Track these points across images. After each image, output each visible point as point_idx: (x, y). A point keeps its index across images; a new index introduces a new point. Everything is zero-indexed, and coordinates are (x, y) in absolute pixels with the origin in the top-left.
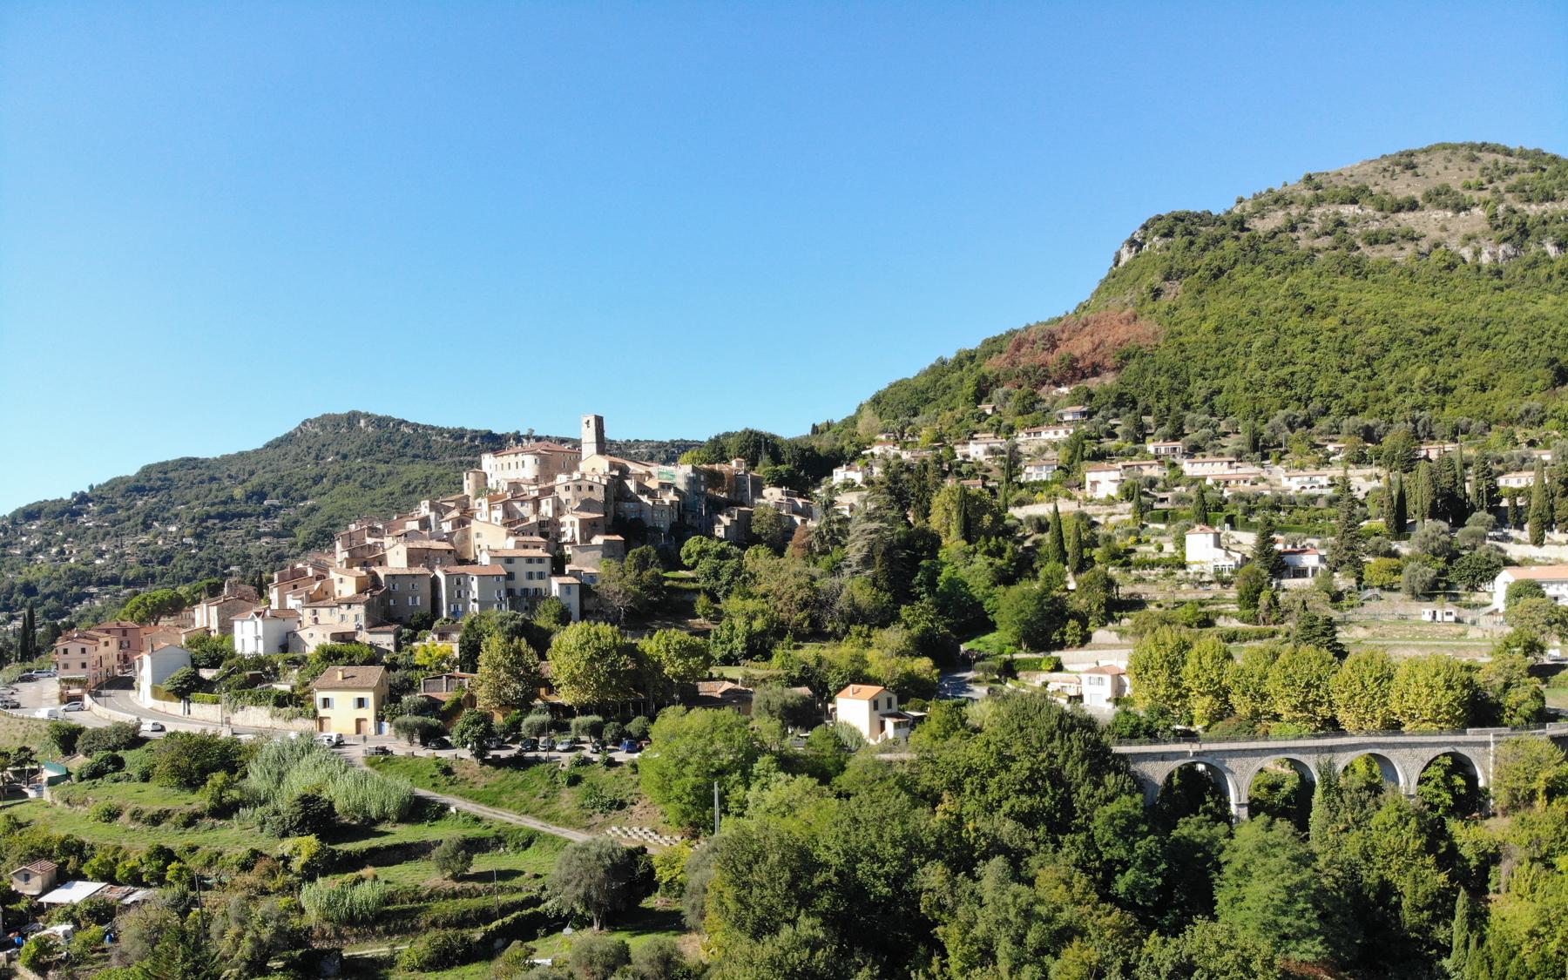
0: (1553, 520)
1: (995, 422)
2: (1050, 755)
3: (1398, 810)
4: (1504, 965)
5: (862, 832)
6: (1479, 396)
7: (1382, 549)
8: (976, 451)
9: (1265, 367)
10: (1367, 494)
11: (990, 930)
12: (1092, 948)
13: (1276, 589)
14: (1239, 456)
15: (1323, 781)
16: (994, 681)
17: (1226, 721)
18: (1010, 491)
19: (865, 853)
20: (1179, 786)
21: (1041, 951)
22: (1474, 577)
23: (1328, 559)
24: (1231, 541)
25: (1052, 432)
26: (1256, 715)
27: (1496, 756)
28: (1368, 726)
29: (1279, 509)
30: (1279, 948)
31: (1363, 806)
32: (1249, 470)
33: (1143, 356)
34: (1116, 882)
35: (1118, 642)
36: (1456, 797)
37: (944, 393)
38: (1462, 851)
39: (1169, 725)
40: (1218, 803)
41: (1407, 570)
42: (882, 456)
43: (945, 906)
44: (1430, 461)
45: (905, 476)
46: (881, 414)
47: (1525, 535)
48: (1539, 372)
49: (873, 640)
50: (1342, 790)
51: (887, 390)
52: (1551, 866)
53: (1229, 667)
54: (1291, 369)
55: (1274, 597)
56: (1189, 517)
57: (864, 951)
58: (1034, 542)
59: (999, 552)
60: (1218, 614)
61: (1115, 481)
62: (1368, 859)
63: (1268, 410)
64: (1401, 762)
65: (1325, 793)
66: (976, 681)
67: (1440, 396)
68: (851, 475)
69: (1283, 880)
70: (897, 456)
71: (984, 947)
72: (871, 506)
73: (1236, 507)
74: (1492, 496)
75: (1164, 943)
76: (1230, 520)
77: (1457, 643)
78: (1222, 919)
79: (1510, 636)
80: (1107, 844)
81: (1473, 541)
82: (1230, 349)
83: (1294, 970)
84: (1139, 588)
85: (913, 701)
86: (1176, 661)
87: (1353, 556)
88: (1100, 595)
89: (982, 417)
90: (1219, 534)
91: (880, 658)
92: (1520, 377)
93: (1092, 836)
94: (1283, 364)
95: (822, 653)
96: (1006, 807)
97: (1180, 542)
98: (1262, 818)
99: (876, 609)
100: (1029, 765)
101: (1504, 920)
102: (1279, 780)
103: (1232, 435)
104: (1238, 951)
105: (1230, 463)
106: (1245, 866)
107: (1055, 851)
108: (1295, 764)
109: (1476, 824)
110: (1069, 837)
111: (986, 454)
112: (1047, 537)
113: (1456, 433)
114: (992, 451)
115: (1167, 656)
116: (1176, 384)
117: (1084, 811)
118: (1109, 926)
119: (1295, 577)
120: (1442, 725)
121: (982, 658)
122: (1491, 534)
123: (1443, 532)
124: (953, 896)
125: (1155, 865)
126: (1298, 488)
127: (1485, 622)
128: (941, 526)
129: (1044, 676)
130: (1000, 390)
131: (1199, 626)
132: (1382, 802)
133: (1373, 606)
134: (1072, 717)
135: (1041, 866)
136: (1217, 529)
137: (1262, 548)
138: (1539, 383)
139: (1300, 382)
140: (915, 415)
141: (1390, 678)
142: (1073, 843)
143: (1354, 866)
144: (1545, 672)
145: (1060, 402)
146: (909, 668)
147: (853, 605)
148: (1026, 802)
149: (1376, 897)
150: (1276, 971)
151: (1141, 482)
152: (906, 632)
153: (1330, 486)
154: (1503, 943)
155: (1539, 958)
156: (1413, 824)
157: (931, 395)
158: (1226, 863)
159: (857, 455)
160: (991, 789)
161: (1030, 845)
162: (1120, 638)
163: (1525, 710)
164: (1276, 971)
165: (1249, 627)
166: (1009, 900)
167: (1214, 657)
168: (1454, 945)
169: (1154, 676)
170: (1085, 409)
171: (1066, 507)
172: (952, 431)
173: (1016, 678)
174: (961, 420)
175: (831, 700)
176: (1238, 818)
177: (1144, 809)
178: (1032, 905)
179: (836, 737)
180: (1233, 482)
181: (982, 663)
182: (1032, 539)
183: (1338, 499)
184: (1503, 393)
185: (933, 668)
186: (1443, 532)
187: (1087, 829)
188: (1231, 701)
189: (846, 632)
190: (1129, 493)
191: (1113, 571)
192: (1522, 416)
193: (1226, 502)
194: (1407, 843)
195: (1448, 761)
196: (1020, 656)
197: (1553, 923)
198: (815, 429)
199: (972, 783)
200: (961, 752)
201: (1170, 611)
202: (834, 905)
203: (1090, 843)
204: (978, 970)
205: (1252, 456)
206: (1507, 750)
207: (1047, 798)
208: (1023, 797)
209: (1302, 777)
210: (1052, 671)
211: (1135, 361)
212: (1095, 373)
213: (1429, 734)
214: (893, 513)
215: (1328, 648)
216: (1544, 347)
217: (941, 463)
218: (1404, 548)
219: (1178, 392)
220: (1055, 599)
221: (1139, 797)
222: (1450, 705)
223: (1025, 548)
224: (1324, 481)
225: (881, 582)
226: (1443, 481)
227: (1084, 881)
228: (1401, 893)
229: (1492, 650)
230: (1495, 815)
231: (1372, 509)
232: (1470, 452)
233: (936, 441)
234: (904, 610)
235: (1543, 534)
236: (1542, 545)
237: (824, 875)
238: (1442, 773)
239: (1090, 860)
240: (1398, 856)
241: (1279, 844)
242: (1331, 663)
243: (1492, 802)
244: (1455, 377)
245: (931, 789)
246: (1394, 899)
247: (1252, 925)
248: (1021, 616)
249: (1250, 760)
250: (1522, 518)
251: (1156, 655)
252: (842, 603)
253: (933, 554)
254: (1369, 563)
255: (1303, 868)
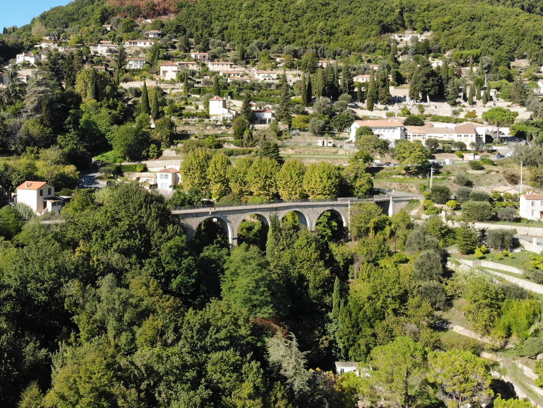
0: (378, 99)
1: (112, 35)
2: (140, 217)
3: (307, 238)
4: (357, 314)
5: (30, 266)
6: (347, 38)
7: (300, 111)
8: (102, 50)
9: (249, 17)
10: (294, 83)
11: (104, 315)
12: (159, 319)
13: (252, 130)
14: (235, 62)
15: (272, 225)
16: (111, 178)
17: (227, 196)
18: (120, 74)
19: (32, 278)
20: (204, 230)
21: (131, 324)
22: (341, 125)
23: (276, 115)
24: (231, 104)
25: (142, 43)
26: (241, 193)
27: (351, 211)
28: (294, 197)
29: (254, 90)
30: (252, 312)
31: (291, 236)
32: (240, 69)
33: (189, 6)
34: (171, 283)
35: (176, 156)
36: (333, 232)
37: (83, 16)
38: (336, 258)
39: (200, 199)
40: (223, 238)
41: (311, 121)
42: (47, 49)
43: (78, 304)
44: (323, 68)
45: (60, 61)
46: (46, 25)
47: (365, 105)
48: (374, 27)
49: (40, 155)
50: (281, 229)
51: (50, 12)
52: (377, 265)
53: (229, 169)
54: (261, 19)
55: (251, 134)
56: (211, 92)
57: (31, 333)
58: (133, 102)
59: (114, 107)
60: (224, 142)
61: (175, 71)
62: (293, 264)
63: (249, 39)
64: (308, 215)
65: (274, 231)
66: (101, 178)
67: (328, 36)
68: (28, 59)
69: (254, 276)
70: (56, 50)
71: (100, 325)
72: (40, 77)
73: (233, 88)
74: (351, 85)
75: (196, 313)
76: (231, 94)
77: (333, 157)
78: (224, 298)
79: (357, 153)
80: (168, 263)
81: (341, 107)
82: (232, 6)
83: (259, 323)
84: (186, 128)
85: (64, 190)
86: (204, 166)
87: (287, 114)
88: (167, 131)
89: (105, 32)
90: (225, 101)
91: (44, 165)
92: (365, 29)
93: (160, 259)
94: (257, 16)
95: (8, 162)
96: (115, 246)
97: (207, 105)
98: (244, 245)
99: (42, 137)
100: (128, 222)
101: (356, 292)
102: (252, 225)
103: (232, 51)
104: (232, 315)
105: (231, 65)
106: (236, 270)
107: (140, 269)
108: (260, 217)
109: (342, 244)
110: (148, 260)
111: (107, 52)
112: (140, 99)
113: (335, 55)
114: (110, 51)
115: (200, 163)
116: (205, 23)
117: (156, 246)
118: (168, 307)
119: (261, 123)
120: (326, 196)
121: (104, 165)
122: (349, 104)
123: (328, 103)
124: (84, 298)
125: (191, 272)
126: (262, 79)
127: (346, 146)
128: (82, 91)
129: (138, 174)
130: (115, 18)
131: (215, 148)
132: (299, 235)
133: (296, 139)
134: (152, 196)
135: (133, 277)
136: (225, 98)
137: (245, 109)
138: (374, 32)
139: (264, 26)
140: (67, 27)
141: (303, 174)
142: (150, 263)
143: (286, 267)
144: (373, 171)
145: (147, 27)
146: (62, 171)
147: (28, 134)
148: (126, 243)
149: (297, 283)
150: (250, 324)
151: (188, 72)
152: (60, 151)
153: (278, 79)
154: (356, 303)
155: (373, 310)
156: (314, 245)
157: (76, 17)
158: (226, 269)
159: (31, 48)
160: (107, 237)
161: (127, 266)
162: (177, 154)
163: (363, 189)
164: (250, 324)
165: (239, 148)
166: (116, 297)
167: (222, 164)
168: (334, 305)
169: (194, 173)
170: (160, 32)
171: (150, 84)
172: (89, 38)
173: (123, 176)
174: (93, 32)
175: (13, 190)
176: (232, 245)
177: (187, 243)
178: (127, 299)
179: (16, 212)
180: (232, 75)
181: (104, 168)
182: (132, 100)
183: (281, 85)
184: (357, 37)
185: (76, 171)
186: (328, 103)
187: (158, 255)
188: (230, 186)
189: (24, 150)
190: (182, 78)
191: (174, 119)
192: (365, 48)
193: (229, 85)
194: (311, 255)
195: (329, 214)
196: (125, 163)
197: (379, 292)
198: (5, 31)
199: (97, 234)
200: (91, 217)
201: (201, 140)
202: (13, 309)
203: (159, 263)
204: (97, 337)
205: (241, 62)
206: (356, 208)
207: (137, 240)
208: (124, 241)
209: (263, 223)
210: (142, 171)
211: (186, 9)
212: (165, 13)
213: (323, 201)
214: (53, 82)
215: (275, 159)
216: (377, 15)
217: (82, 55)
218: (310, 110)
219: (206, 27)
220: (144, 133)
221: (184, 236)
222: (330, 187)
223: (128, 105)
224: (275, 76)
225: (45, 122)
226: (328, 78)
227: (155, 284)
228: (309, 280)
229: (349, 160)
230: (351, 240)
231: (296, 91)
232: (341, 65)
233: (79, 43)
234: (59, 138)
235: (373, 105)
236: (372, 110)
237: (7, 291)
238: (326, 219)
239: (158, 272)
240: (307, 261)
241: (252, 257)
242: (277, 166)
243: (349, 234)
244: (336, 27)
245: (73, 239)
246: (305, 283)
247: (238, 301)
248: (126, 142)
249: (238, 215)
250: (364, 97)
251: (194, 163)
252: (21, 133)
253: (77, 107)
254: (294, 117)
255: (263, 269)
